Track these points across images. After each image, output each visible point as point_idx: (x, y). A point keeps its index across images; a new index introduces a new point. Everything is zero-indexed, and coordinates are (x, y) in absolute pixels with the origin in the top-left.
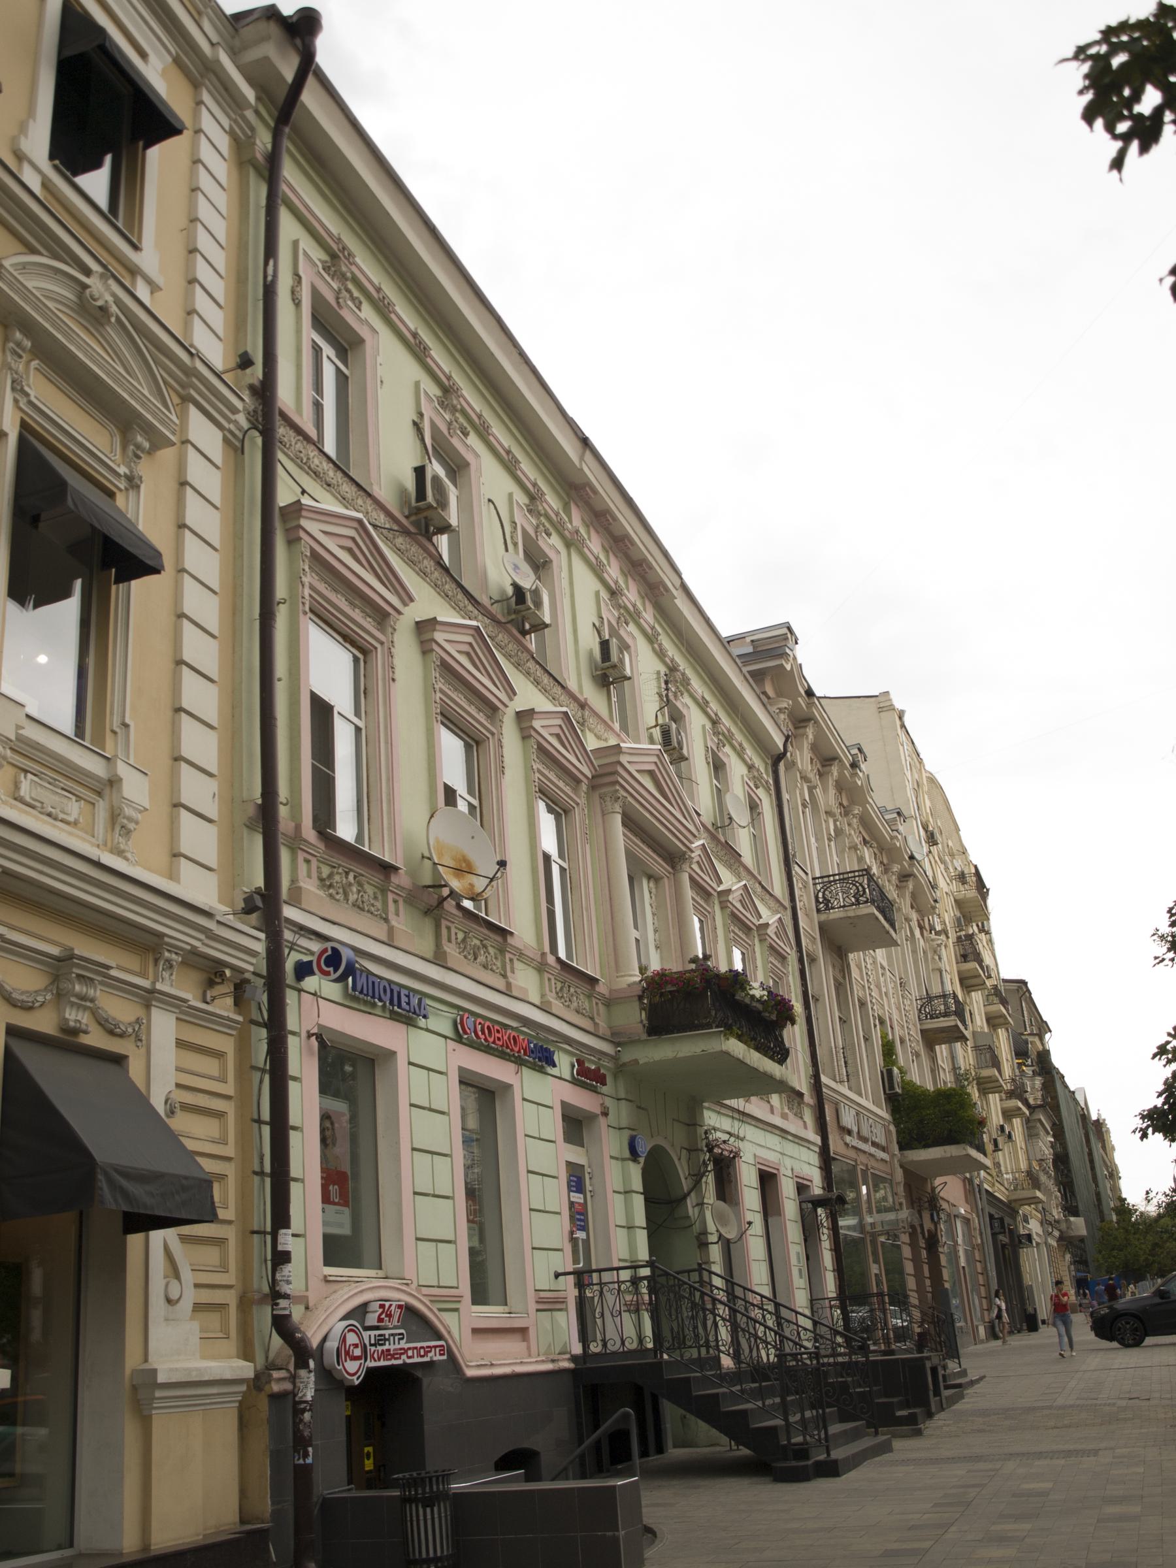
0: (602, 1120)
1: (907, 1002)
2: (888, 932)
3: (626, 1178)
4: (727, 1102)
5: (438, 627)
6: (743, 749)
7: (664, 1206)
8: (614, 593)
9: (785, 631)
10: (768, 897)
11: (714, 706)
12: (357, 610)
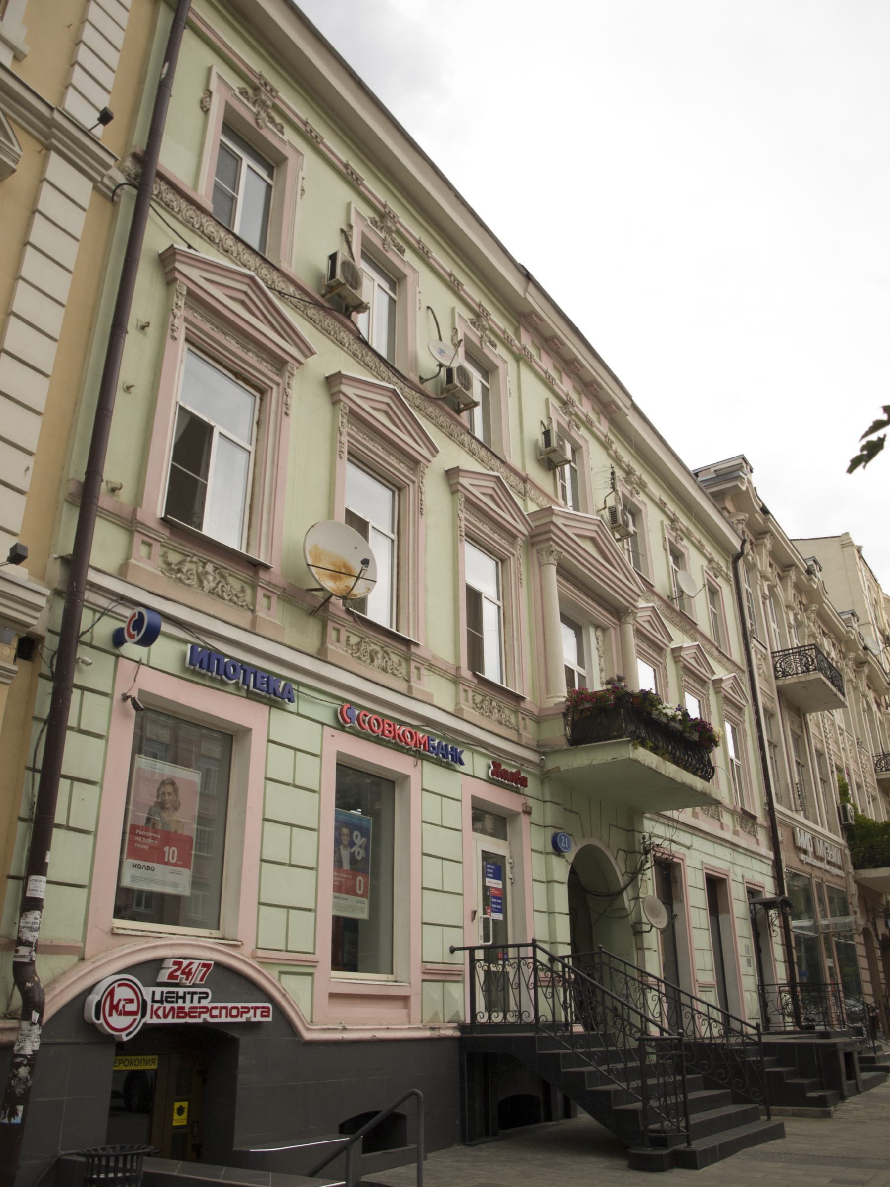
0: (524, 819)
1: (864, 758)
2: (836, 695)
3: (548, 869)
4: (664, 813)
5: (461, 474)
6: (702, 545)
7: (592, 898)
8: (565, 403)
9: (741, 461)
10: (725, 660)
11: (672, 507)
12: (250, 354)
